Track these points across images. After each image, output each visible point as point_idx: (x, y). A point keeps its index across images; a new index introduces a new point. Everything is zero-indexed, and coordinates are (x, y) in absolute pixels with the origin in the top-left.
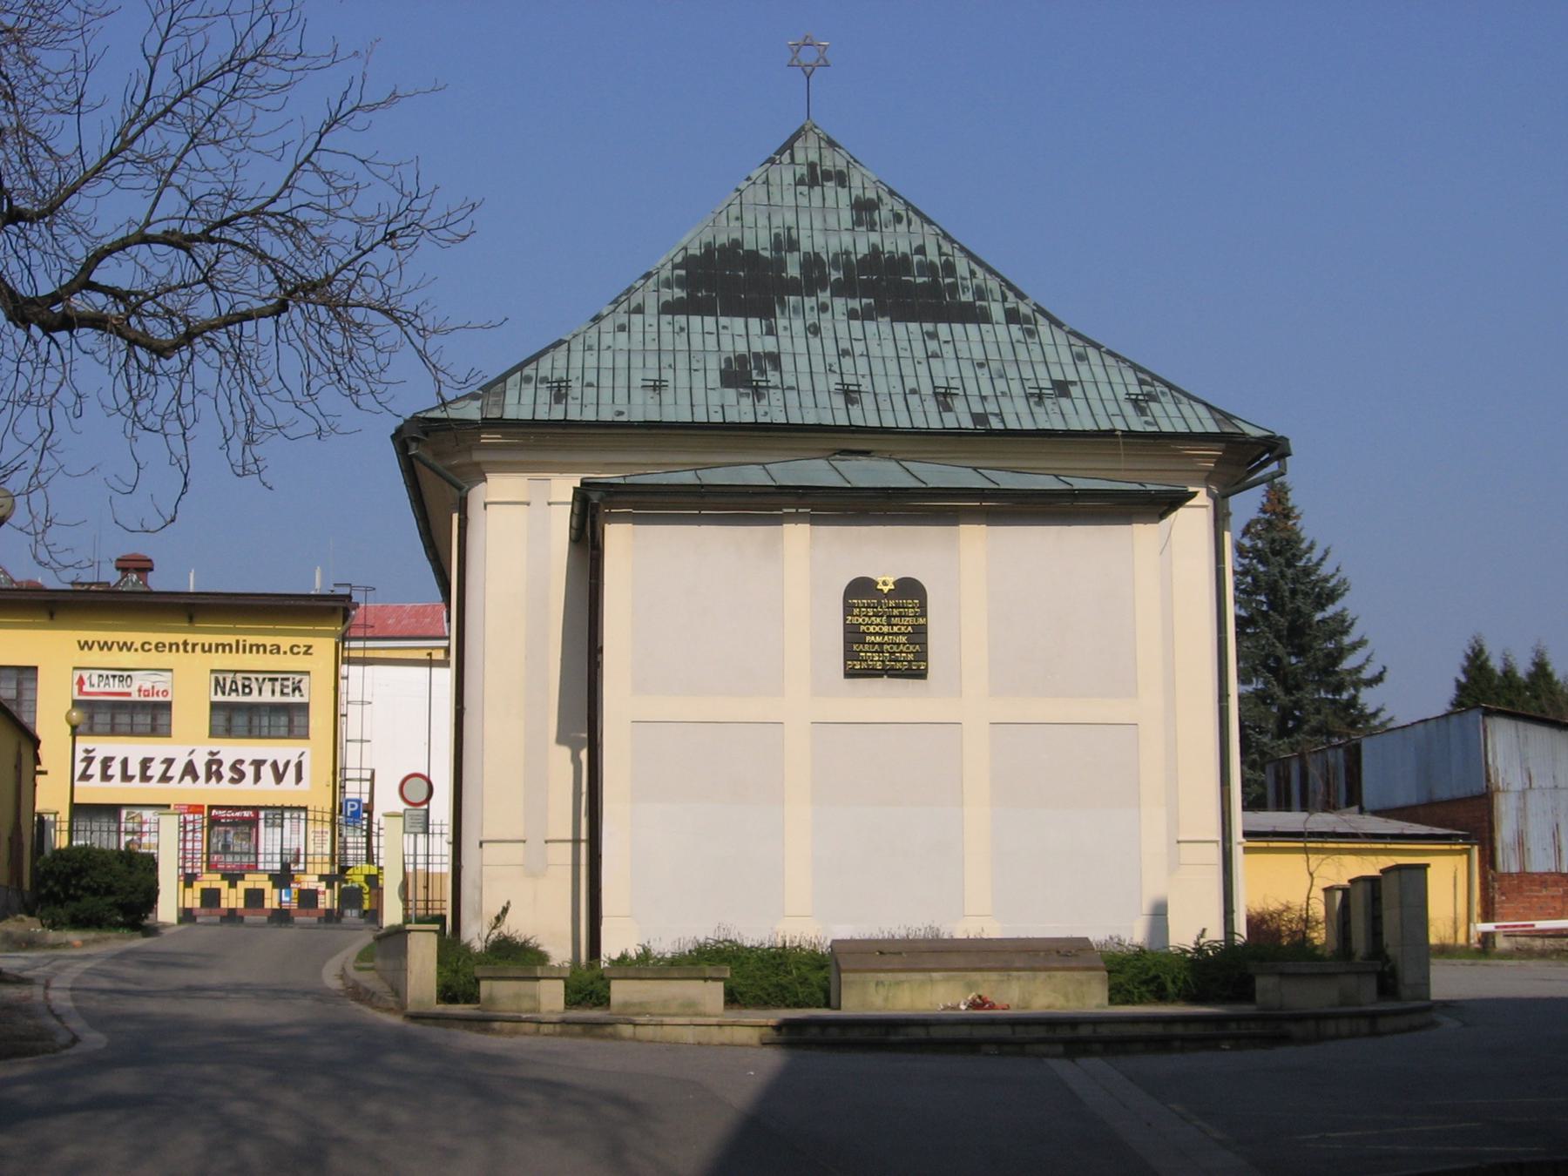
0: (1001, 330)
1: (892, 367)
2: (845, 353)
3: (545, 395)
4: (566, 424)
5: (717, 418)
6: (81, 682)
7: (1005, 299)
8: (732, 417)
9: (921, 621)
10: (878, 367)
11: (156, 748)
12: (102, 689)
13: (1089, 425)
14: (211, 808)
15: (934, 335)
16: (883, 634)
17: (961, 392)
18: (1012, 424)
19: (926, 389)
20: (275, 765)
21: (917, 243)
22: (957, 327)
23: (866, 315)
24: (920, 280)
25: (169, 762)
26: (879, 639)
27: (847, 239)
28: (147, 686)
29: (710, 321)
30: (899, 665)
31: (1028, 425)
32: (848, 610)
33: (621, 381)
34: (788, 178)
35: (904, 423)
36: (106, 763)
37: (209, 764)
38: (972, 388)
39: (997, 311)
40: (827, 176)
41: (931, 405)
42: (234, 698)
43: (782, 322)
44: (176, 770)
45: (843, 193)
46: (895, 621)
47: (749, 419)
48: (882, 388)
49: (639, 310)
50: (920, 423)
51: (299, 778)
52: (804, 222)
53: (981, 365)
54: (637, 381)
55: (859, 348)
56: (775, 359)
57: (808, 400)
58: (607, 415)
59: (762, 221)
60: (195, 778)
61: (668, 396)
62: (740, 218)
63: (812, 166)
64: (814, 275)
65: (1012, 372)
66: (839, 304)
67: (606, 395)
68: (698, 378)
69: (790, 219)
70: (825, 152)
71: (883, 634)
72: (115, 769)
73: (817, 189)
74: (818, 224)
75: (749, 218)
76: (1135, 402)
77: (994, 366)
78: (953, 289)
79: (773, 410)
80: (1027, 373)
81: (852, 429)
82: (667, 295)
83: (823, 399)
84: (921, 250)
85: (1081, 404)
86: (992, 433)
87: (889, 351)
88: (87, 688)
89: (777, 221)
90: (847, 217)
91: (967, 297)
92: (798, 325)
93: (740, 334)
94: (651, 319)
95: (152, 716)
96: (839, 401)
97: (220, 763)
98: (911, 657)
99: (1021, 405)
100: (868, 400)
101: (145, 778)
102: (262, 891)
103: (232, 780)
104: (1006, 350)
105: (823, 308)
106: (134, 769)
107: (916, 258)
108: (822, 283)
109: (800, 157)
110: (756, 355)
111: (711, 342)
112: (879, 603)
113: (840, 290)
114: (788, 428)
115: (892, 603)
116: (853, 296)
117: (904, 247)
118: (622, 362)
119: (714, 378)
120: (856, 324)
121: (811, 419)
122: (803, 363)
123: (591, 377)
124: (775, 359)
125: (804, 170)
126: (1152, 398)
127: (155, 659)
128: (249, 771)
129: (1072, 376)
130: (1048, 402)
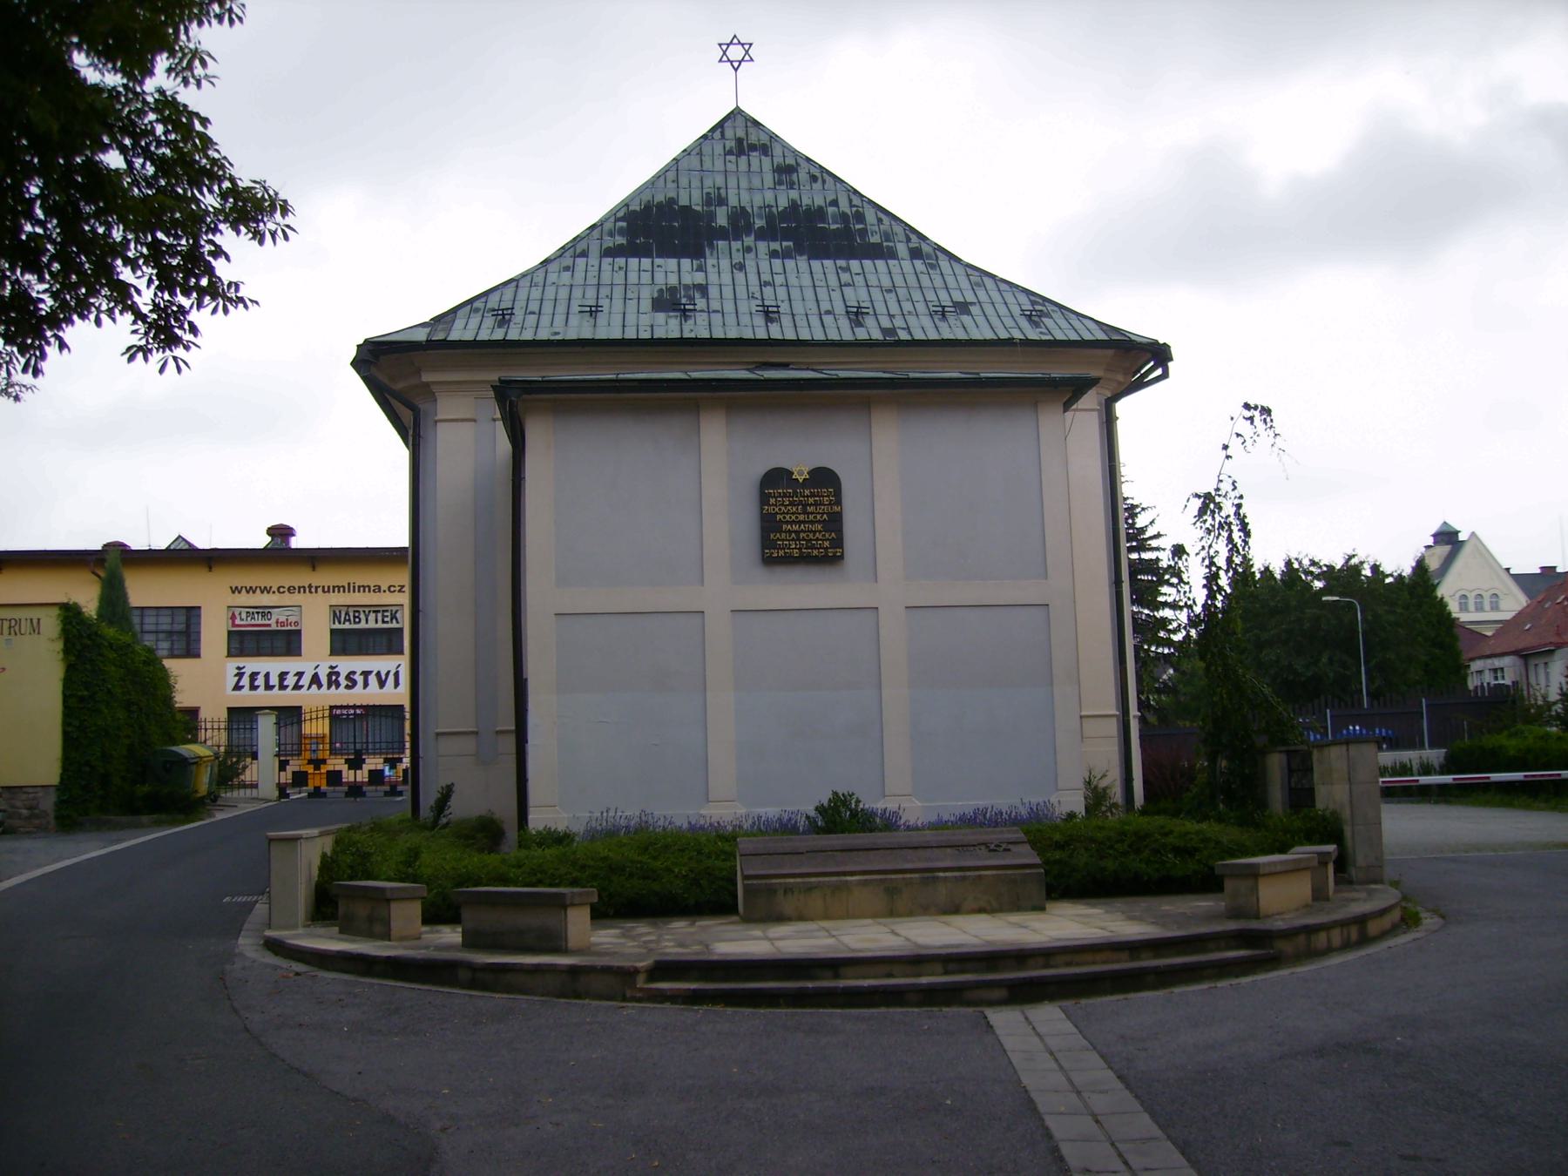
0: (907, 265)
1: (809, 294)
2: (767, 284)
3: (489, 321)
4: (505, 344)
5: (645, 335)
6: (233, 617)
7: (909, 240)
8: (660, 333)
9: (836, 509)
10: (795, 293)
11: (290, 665)
12: (250, 621)
13: (989, 335)
14: (332, 708)
15: (847, 269)
16: (800, 522)
17: (871, 311)
18: (919, 335)
19: (839, 308)
20: (378, 674)
21: (830, 197)
22: (867, 263)
23: (786, 255)
24: (834, 227)
25: (300, 675)
26: (796, 528)
27: (769, 197)
28: (282, 619)
29: (646, 262)
30: (815, 552)
31: (933, 335)
32: (764, 499)
33: (561, 309)
34: (719, 149)
35: (819, 336)
36: (254, 676)
37: (330, 675)
38: (880, 308)
39: (902, 249)
40: (753, 148)
41: (844, 323)
42: (347, 626)
43: (711, 261)
44: (305, 681)
45: (766, 161)
46: (810, 509)
47: (676, 335)
48: (798, 308)
49: (584, 254)
50: (833, 335)
51: (397, 684)
52: (732, 182)
53: (889, 291)
54: (575, 308)
55: (779, 279)
56: (703, 289)
57: (730, 320)
58: (543, 335)
59: (696, 183)
60: (320, 686)
61: (602, 319)
62: (676, 181)
63: (739, 141)
64: (740, 223)
65: (917, 296)
66: (762, 246)
67: (545, 320)
68: (632, 305)
69: (720, 181)
70: (751, 130)
71: (800, 522)
72: (260, 681)
73: (744, 158)
74: (744, 184)
75: (684, 181)
76: (1029, 317)
77: (902, 292)
78: (863, 233)
79: (698, 328)
80: (931, 296)
81: (770, 342)
82: (609, 242)
83: (745, 319)
84: (835, 203)
85: (981, 320)
86: (900, 343)
87: (806, 281)
88: (238, 622)
89: (708, 183)
90: (769, 179)
91: (875, 239)
92: (725, 264)
93: (672, 271)
94: (594, 260)
95: (288, 642)
96: (759, 320)
97: (338, 674)
98: (827, 544)
99: (926, 321)
100: (786, 321)
101: (283, 687)
102: (340, 772)
103: (347, 687)
104: (912, 280)
105: (749, 250)
106: (274, 680)
107: (831, 210)
108: (748, 228)
109: (729, 133)
110: (687, 287)
111: (646, 277)
112: (795, 493)
113: (762, 235)
114: (712, 342)
115: (807, 492)
116: (774, 239)
117: (819, 201)
118: (563, 293)
119: (646, 305)
120: (777, 263)
121: (732, 334)
122: (728, 292)
123: (534, 306)
124: (703, 289)
125: (733, 144)
126: (1042, 314)
127: (287, 599)
128: (359, 679)
129: (970, 298)
130: (951, 319)
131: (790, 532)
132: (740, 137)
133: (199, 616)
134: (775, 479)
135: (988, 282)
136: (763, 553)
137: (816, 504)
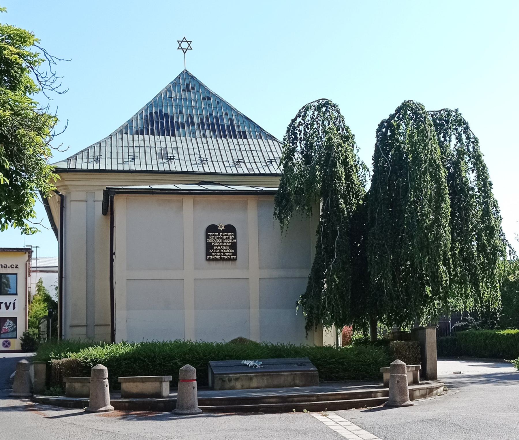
9: (235, 241)
16: (221, 246)
20: (6, 304)
26: (219, 248)
30: (226, 257)
35: (224, 171)
71: (221, 246)
79: (175, 167)
131: (217, 249)
132: (187, 82)
133: (236, 245)
134: (212, 229)
135: (230, 108)
136: (207, 257)
137: (227, 239)
